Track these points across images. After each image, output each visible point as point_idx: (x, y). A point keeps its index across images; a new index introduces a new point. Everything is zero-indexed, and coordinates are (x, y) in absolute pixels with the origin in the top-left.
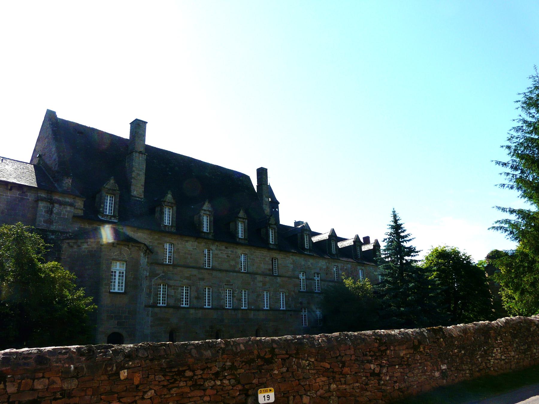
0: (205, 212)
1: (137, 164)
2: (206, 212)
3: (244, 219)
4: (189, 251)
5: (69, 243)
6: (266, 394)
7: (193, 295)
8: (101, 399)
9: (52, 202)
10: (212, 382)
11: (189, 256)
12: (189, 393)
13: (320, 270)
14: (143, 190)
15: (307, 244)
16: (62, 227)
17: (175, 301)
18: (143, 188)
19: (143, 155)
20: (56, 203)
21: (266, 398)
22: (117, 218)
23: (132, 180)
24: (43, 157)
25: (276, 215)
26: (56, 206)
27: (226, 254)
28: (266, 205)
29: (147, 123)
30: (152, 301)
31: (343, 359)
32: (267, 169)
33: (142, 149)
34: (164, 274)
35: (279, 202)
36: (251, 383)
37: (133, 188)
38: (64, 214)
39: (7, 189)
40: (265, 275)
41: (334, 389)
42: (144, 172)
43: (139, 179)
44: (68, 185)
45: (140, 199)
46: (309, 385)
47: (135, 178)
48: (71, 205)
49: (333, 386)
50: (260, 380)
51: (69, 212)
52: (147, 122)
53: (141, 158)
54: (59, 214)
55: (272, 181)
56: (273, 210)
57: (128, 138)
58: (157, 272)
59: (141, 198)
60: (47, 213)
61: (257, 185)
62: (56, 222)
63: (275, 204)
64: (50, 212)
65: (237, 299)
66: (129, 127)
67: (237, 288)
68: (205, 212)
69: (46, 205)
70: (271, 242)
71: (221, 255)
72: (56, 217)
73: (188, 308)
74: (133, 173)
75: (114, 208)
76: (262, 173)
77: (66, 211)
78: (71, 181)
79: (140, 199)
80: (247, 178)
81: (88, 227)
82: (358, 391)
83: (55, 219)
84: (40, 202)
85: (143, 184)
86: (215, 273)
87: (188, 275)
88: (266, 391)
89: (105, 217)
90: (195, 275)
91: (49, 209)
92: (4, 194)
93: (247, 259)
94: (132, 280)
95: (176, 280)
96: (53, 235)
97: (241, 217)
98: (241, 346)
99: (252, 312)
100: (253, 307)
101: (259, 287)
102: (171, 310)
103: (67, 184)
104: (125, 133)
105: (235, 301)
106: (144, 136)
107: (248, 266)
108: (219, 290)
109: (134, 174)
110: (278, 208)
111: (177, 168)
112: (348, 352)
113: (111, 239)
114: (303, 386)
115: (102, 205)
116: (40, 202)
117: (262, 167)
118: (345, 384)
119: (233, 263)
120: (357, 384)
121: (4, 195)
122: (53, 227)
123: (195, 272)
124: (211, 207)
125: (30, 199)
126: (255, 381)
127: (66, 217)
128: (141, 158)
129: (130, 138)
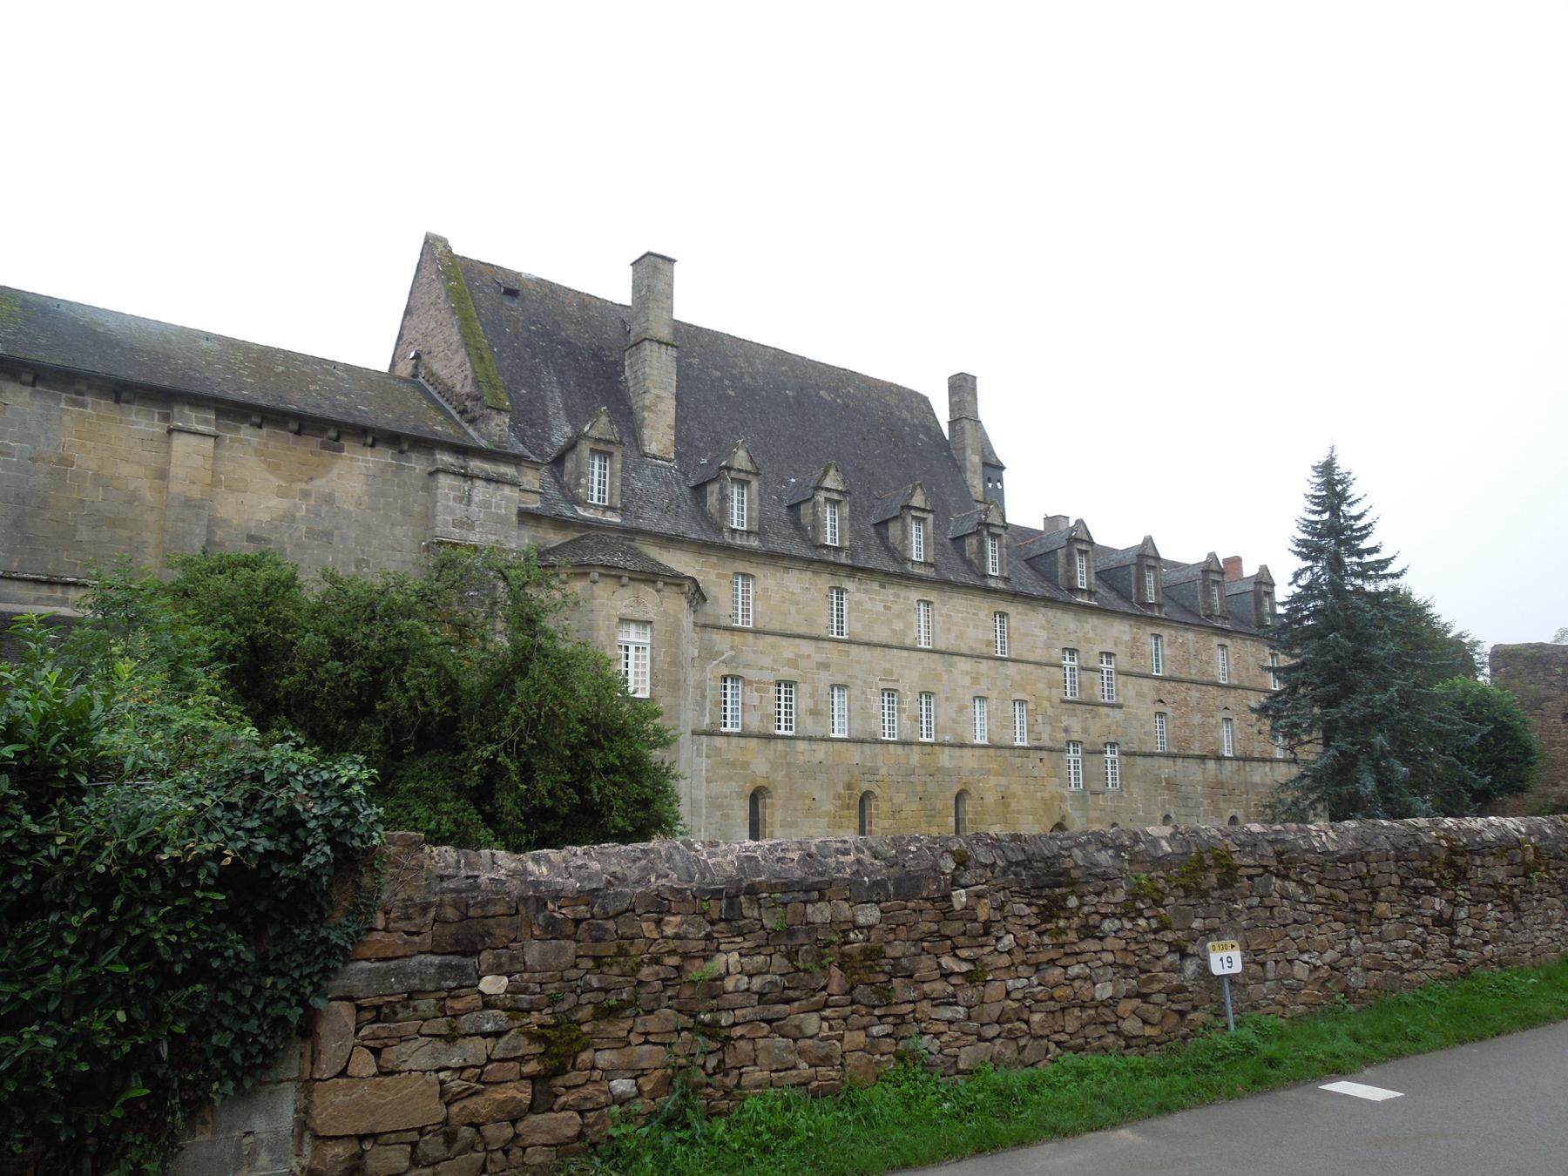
0: (828, 495)
1: (655, 372)
4: (793, 594)
6: (1225, 955)
7: (803, 706)
8: (923, 949)
10: (1116, 922)
11: (793, 609)
12: (1075, 943)
13: (1116, 645)
15: (993, 564)
17: (762, 720)
21: (1226, 964)
23: (646, 414)
24: (425, 358)
25: (996, 499)
27: (882, 601)
28: (975, 472)
29: (675, 261)
30: (707, 720)
31: (1376, 882)
33: (664, 333)
34: (733, 653)
35: (1005, 464)
36: (1189, 928)
37: (647, 433)
38: (499, 507)
40: (978, 657)
41: (1357, 950)
46: (1307, 937)
48: (513, 484)
49: (1355, 943)
50: (1207, 921)
51: (508, 499)
53: (664, 356)
54: (486, 505)
55: (990, 412)
56: (990, 485)
57: (629, 302)
58: (718, 647)
59: (669, 461)
60: (461, 502)
62: (482, 525)
63: (993, 468)
65: (909, 718)
66: (629, 271)
67: (910, 690)
68: (828, 495)
70: (991, 573)
71: (868, 605)
73: (931, 745)
74: (647, 396)
75: (611, 490)
76: (962, 388)
78: (507, 420)
80: (920, 402)
82: (1407, 956)
83: (479, 519)
86: (854, 649)
87: (792, 656)
88: (1225, 948)
90: (809, 656)
93: (933, 616)
94: (666, 667)
95: (761, 668)
98: (1164, 843)
99: (947, 749)
100: (947, 738)
101: (963, 687)
102: (753, 743)
104: (617, 289)
105: (904, 720)
106: (670, 296)
107: (937, 630)
108: (864, 693)
109: (648, 399)
110: (1000, 480)
111: (747, 379)
112: (1384, 867)
113: (1040, 616)
114: (1293, 940)
115: (583, 481)
118: (1380, 939)
119: (898, 625)
120: (1405, 942)
123: (807, 647)
126: (1197, 924)
128: (664, 356)
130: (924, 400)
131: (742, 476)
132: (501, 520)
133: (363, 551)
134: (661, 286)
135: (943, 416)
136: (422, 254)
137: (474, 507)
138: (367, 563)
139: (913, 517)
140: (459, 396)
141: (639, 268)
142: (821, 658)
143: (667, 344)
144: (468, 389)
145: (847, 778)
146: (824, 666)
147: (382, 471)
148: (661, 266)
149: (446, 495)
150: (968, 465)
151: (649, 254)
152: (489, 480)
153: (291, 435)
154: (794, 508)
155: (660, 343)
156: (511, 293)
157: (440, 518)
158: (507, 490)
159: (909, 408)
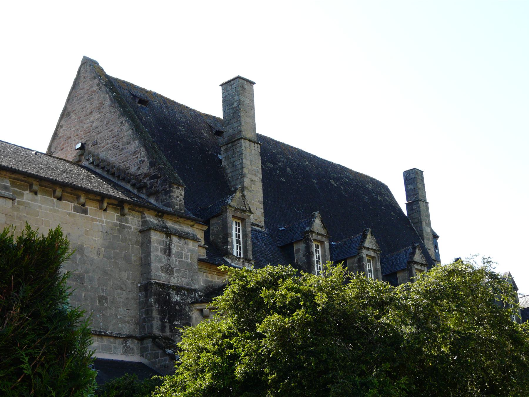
2: (369, 251)
3: (422, 265)
5: (201, 311)
9: (168, 233)
14: (263, 211)
16: (186, 280)
18: (262, 206)
19: (256, 144)
20: (174, 234)
22: (253, 263)
26: (175, 239)
29: (254, 83)
32: (422, 172)
39: (101, 208)
42: (261, 176)
43: (254, 191)
44: (180, 201)
45: (260, 229)
47: (249, 188)
51: (192, 251)
52: (255, 82)
59: (262, 227)
61: (406, 202)
64: (168, 251)
69: (160, 239)
72: (176, 261)
77: (189, 251)
78: (183, 193)
79: (260, 229)
81: (217, 280)
84: (152, 233)
85: (262, 200)
89: (236, 261)
91: (166, 245)
92: (98, 218)
96: (177, 294)
97: (418, 263)
103: (178, 199)
116: (152, 233)
117: (415, 168)
121: (96, 221)
122: (175, 281)
124: (376, 242)
125: (132, 227)
127: (189, 260)
129: (224, 111)
130: (385, 188)
131: (319, 238)
132: (189, 266)
133: (103, 290)
134: (247, 101)
135: (401, 199)
136: (79, 72)
137: (173, 258)
138: (106, 298)
139: (417, 269)
140: (137, 177)
141: (229, 88)
143: (254, 143)
144: (145, 169)
147: (112, 229)
148: (246, 87)
149: (156, 248)
150: (425, 234)
151: (239, 77)
153: (55, 200)
154: (489, 257)
155: (250, 141)
156: (143, 102)
157: (153, 265)
159: (380, 193)
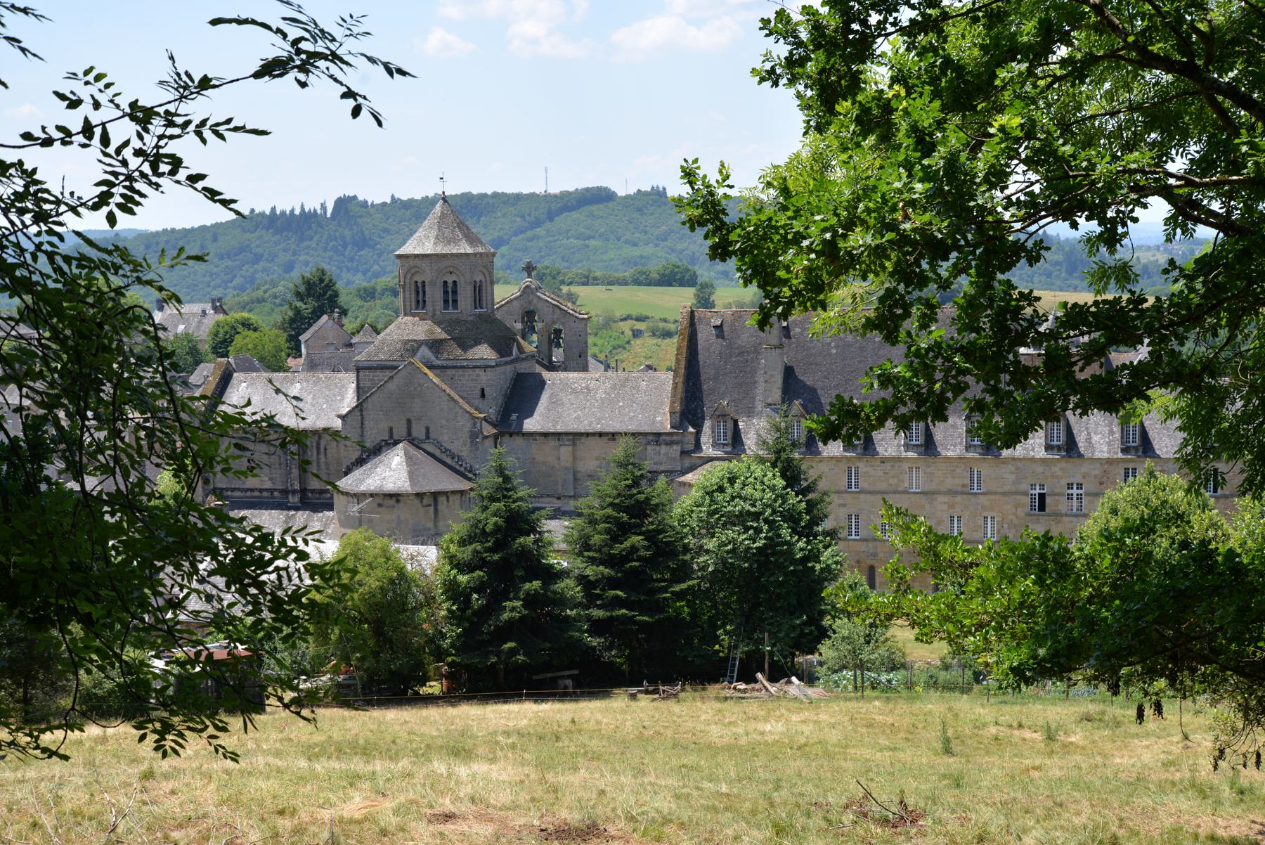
54: (666, 454)
142: (841, 502)
145: (857, 558)
146: (844, 505)
152: (667, 444)
158: (675, 447)
